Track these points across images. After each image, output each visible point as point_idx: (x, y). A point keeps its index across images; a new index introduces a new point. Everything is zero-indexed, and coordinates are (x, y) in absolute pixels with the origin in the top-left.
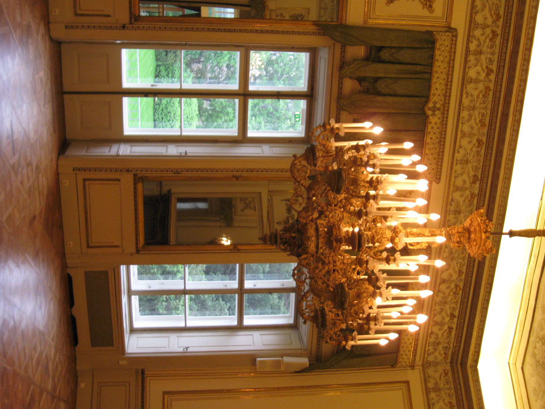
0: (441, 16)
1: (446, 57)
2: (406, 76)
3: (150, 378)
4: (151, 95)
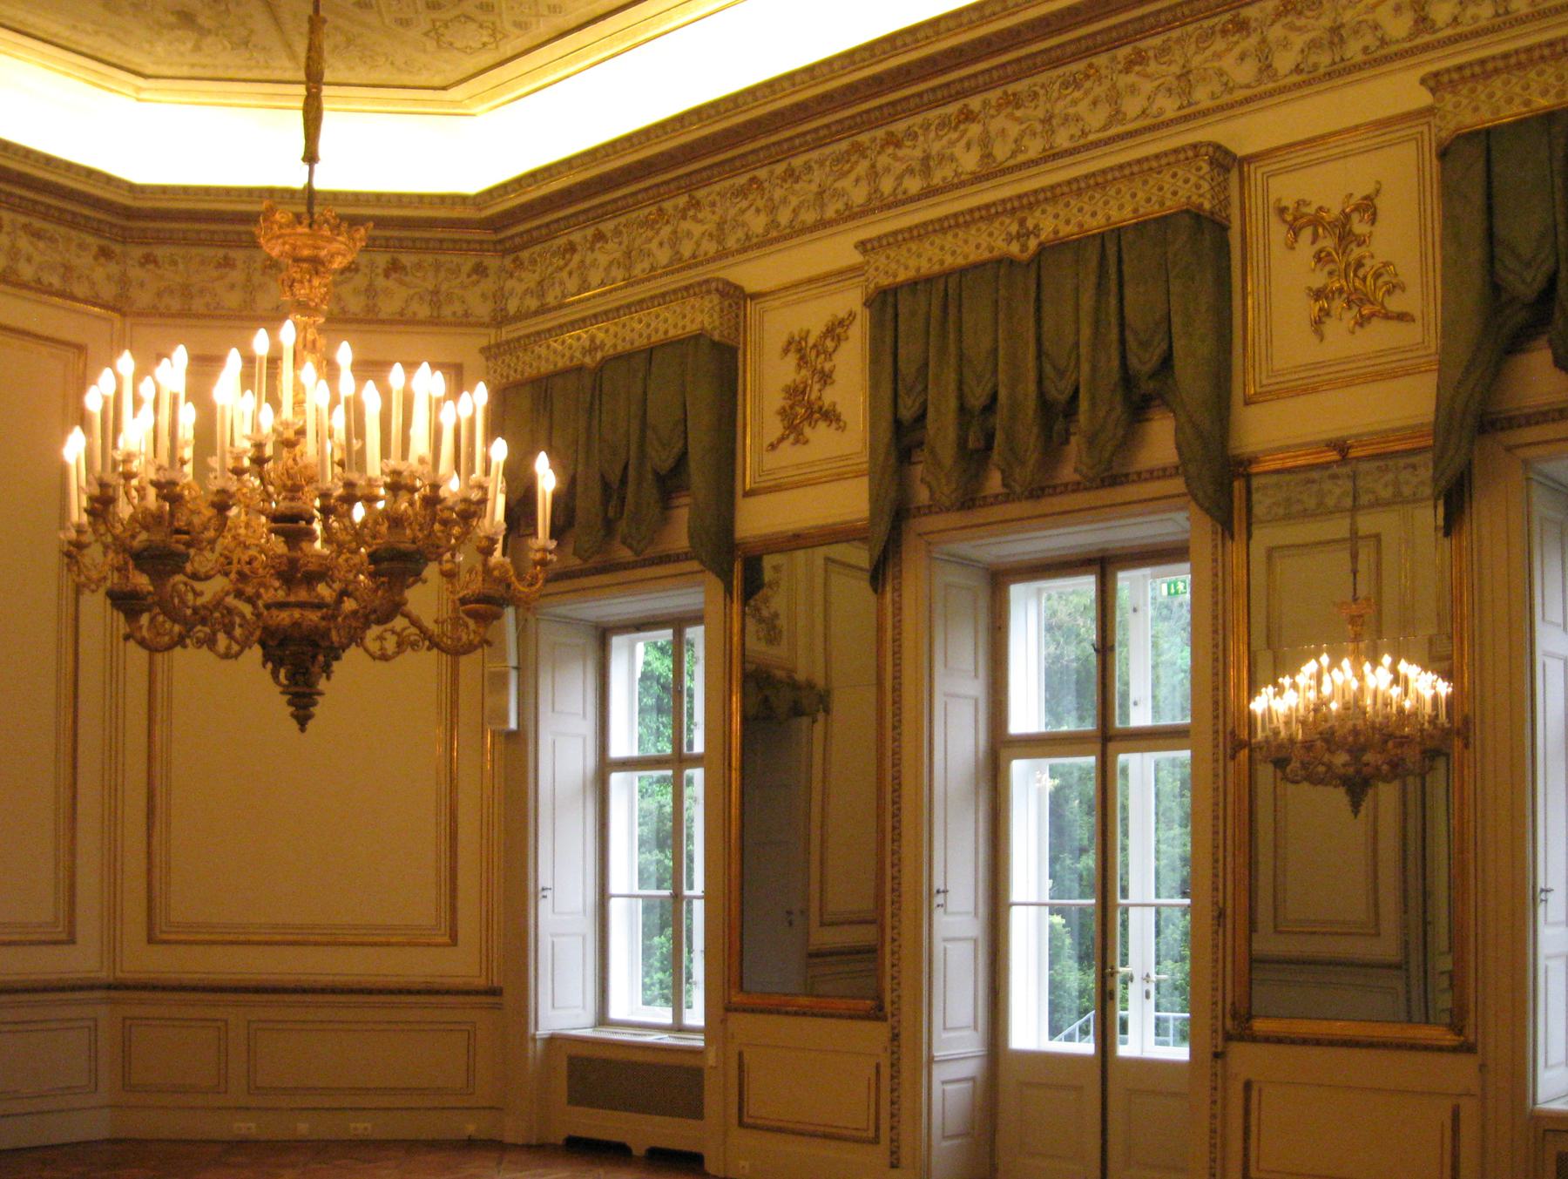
0: (1270, 181)
1: (909, 250)
4: (1109, 983)
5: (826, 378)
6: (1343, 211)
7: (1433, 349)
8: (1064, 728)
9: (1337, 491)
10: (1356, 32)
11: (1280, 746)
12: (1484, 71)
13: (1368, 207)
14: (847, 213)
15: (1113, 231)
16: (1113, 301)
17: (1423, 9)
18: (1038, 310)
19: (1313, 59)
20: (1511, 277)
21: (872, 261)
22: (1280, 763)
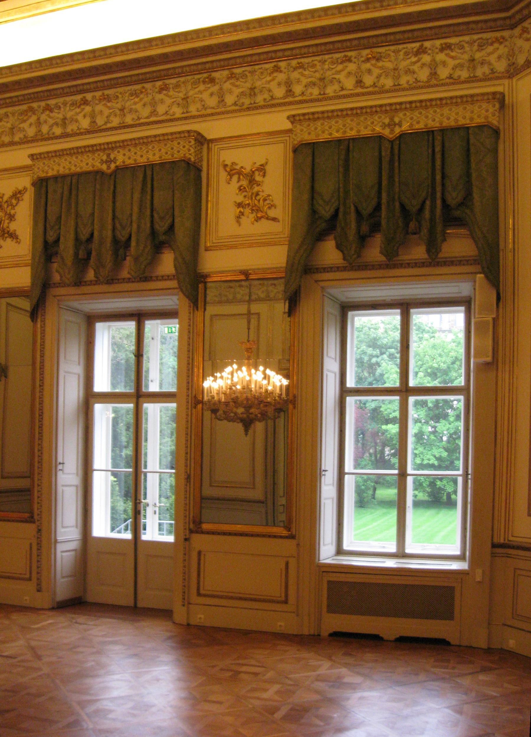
1: (54, 162)
2: (73, 205)
3: (510, 535)
5: (12, 218)
6: (251, 170)
7: (286, 235)
8: (117, 391)
9: (242, 292)
10: (331, 82)
11: (215, 404)
12: (313, 117)
13: (262, 169)
14: (25, 140)
15: (150, 165)
16: (149, 197)
17: (290, 86)
18: (114, 197)
19: (242, 100)
20: (320, 208)
21: (36, 165)
22: (214, 411)
